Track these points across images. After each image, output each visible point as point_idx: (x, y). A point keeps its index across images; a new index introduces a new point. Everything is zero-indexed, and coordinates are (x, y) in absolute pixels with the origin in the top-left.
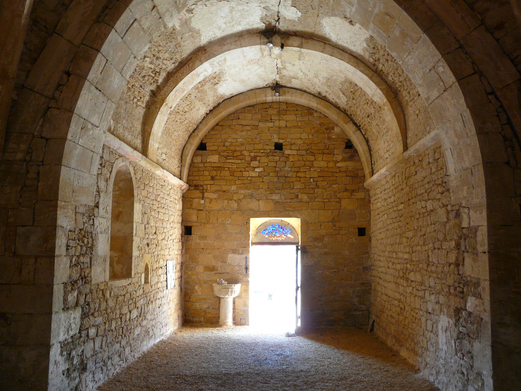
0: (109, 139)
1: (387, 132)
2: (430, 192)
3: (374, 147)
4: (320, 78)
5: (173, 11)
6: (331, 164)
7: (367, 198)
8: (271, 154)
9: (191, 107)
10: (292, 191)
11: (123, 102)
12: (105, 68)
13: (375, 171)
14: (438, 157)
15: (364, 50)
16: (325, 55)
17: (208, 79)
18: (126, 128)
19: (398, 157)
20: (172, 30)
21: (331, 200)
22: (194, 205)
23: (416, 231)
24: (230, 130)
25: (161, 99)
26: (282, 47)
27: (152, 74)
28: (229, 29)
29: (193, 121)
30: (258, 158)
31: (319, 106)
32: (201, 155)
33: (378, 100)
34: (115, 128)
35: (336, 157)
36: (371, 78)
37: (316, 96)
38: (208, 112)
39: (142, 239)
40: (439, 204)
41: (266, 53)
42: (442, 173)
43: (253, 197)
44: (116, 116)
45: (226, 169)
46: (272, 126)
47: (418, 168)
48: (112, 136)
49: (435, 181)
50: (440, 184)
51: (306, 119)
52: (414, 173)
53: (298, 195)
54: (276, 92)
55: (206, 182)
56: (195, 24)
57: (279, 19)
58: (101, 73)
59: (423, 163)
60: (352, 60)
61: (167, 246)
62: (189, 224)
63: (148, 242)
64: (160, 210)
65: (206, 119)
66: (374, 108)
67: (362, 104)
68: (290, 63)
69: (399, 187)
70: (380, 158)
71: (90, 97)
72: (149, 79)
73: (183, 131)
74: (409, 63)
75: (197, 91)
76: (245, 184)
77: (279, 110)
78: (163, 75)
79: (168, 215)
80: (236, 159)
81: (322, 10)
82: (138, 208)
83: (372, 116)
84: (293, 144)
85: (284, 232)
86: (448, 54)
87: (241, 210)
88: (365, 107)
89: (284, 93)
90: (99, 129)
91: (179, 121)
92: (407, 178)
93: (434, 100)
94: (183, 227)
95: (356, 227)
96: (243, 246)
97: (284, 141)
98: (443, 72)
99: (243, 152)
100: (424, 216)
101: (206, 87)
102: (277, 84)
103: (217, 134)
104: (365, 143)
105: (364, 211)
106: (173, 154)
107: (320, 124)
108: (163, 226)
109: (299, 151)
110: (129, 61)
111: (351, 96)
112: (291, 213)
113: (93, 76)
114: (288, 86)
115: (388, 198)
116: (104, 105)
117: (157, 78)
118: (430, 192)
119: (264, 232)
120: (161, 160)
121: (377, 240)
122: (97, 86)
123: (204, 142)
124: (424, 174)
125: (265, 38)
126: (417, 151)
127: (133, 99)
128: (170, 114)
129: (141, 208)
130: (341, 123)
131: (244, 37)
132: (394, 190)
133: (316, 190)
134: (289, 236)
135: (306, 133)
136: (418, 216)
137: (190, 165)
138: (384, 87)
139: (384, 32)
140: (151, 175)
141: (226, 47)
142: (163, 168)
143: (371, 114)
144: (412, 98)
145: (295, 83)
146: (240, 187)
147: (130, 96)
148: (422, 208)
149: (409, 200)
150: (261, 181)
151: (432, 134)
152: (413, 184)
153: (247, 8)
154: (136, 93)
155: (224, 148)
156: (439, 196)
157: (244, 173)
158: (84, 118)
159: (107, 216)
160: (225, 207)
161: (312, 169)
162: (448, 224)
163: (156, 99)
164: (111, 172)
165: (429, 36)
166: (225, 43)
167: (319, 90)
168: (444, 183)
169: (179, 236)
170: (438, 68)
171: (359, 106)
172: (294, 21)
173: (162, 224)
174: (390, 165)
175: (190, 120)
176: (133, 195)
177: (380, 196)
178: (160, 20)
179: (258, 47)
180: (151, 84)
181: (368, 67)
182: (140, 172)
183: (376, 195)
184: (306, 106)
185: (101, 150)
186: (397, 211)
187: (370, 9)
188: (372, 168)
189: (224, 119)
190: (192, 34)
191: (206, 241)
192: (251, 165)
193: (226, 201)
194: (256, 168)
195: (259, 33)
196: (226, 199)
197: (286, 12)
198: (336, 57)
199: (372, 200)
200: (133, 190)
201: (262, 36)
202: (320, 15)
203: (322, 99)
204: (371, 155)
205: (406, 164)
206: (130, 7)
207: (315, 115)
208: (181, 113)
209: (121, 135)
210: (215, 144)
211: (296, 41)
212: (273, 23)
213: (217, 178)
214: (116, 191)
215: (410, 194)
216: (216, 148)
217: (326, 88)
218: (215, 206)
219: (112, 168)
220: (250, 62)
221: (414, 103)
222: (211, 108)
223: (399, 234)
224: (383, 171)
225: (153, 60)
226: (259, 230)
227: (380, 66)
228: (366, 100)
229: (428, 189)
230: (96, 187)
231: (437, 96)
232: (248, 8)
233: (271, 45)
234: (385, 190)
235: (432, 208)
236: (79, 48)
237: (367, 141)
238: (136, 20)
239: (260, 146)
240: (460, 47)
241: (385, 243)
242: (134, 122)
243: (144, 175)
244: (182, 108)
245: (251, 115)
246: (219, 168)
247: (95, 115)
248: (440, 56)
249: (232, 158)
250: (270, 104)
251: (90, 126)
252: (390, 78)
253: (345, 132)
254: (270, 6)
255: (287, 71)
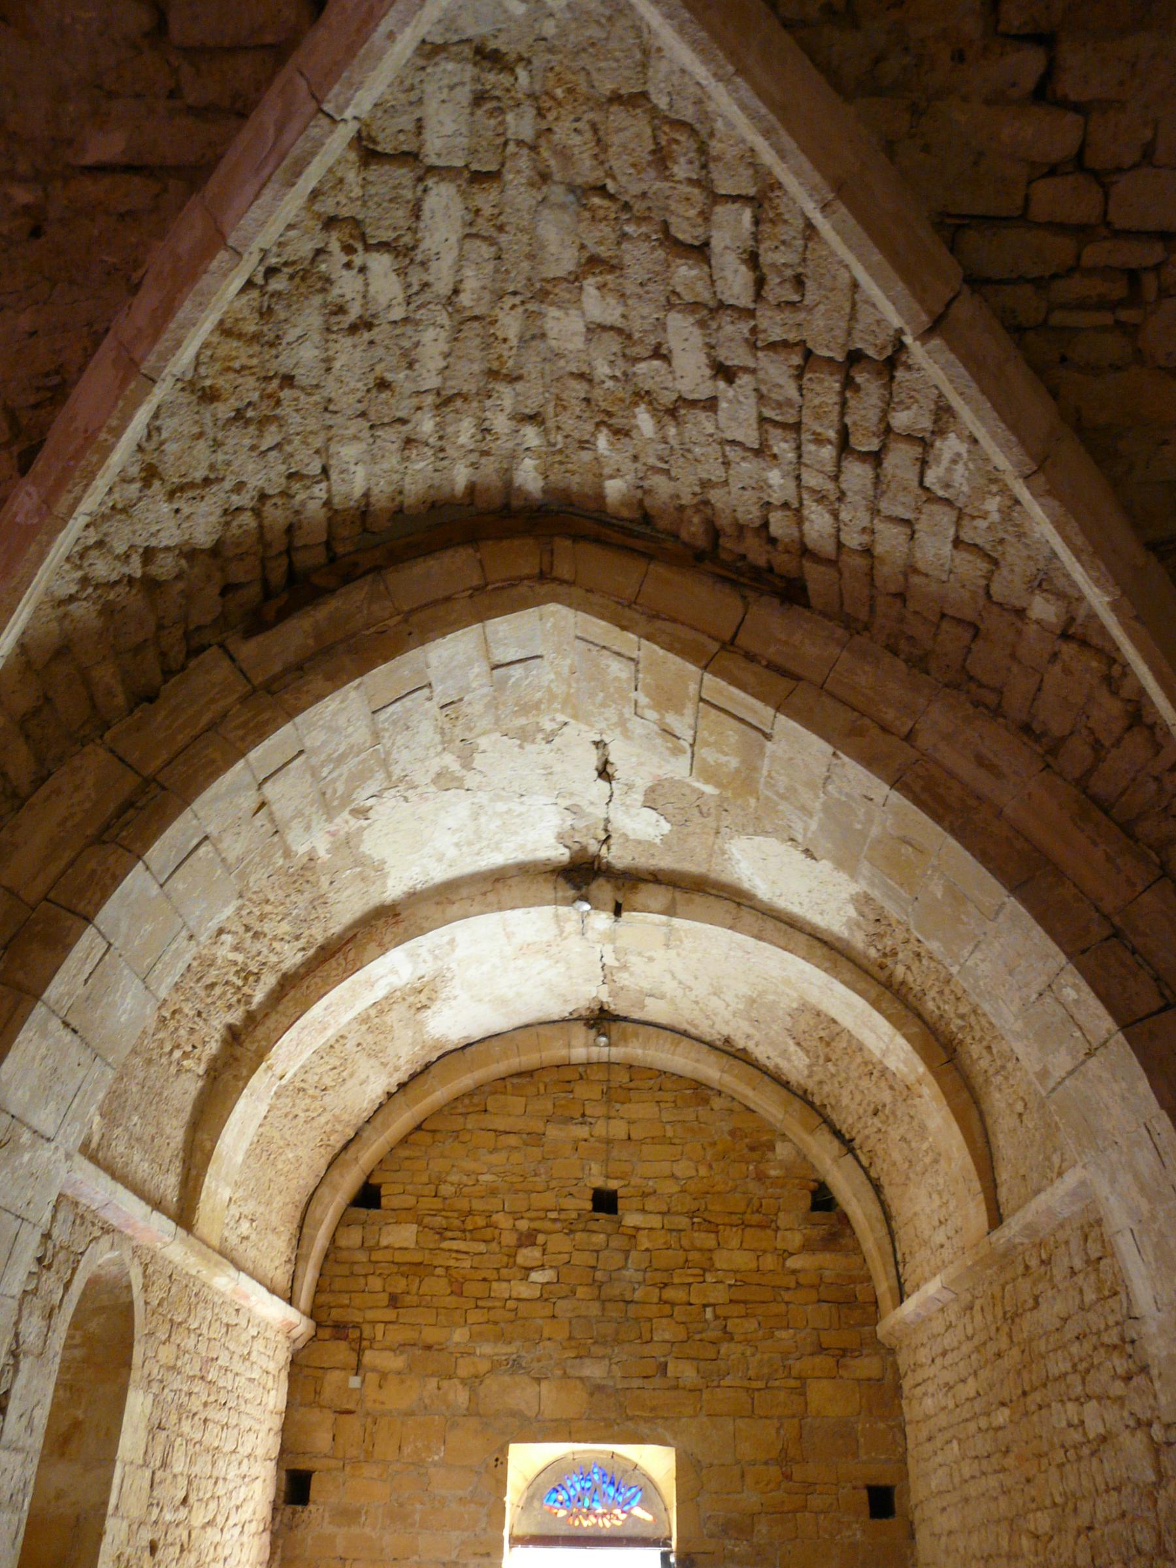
0: (78, 1176)
1: (936, 1161)
2: (1088, 1371)
3: (901, 1208)
4: (729, 997)
5: (314, 817)
6: (769, 1262)
7: (889, 1376)
8: (581, 1226)
9: (344, 1074)
10: (647, 1350)
11: (138, 1061)
12: (100, 968)
13: (907, 1287)
14: (1099, 1254)
15: (851, 924)
16: (739, 937)
17: (398, 994)
18: (138, 1140)
19: (976, 1245)
20: (305, 860)
21: (771, 1383)
22: (328, 1393)
23: (1059, 1510)
24: (456, 1144)
25: (256, 1051)
26: (618, 911)
27: (234, 979)
28: (468, 860)
29: (345, 1117)
30: (541, 1238)
31: (727, 1078)
32: (363, 1224)
33: (901, 1066)
34: (105, 1143)
35: (783, 1240)
36: (875, 1004)
37: (716, 1048)
38: (394, 1090)
39: (135, 1527)
40: (1122, 1418)
41: (571, 927)
42: (1116, 1307)
43: (521, 1367)
44: (110, 1103)
45: (439, 1271)
46: (586, 1136)
47: (1040, 1286)
48: (90, 1168)
49: (1098, 1333)
50: (1115, 1347)
51: (689, 1114)
52: (1031, 1303)
53: (666, 1364)
54: (600, 1034)
55: (371, 1315)
56: (373, 845)
57: (609, 837)
58: (86, 981)
59: (1055, 1272)
60: (819, 952)
61: (219, 1548)
62: (302, 1465)
63: (156, 1537)
64: (212, 1413)
65: (385, 1110)
66: (891, 1088)
67: (854, 1074)
68: (640, 954)
69: (989, 1344)
70: (920, 1246)
71: (43, 1050)
72: (224, 993)
73: (312, 1145)
74: (979, 973)
75: (364, 1027)
76: (496, 1323)
77: (609, 1088)
78: (269, 981)
79: (236, 1431)
80: (473, 1240)
81: (727, 820)
82: (139, 1409)
83: (887, 1111)
84: (649, 1194)
85: (620, 1499)
86: (1083, 952)
87: (478, 1414)
88: (865, 1083)
89: (624, 1039)
90: (53, 1145)
91: (302, 1115)
92: (1012, 1317)
93: (1064, 1079)
94: (284, 1475)
95: (860, 1483)
96: (483, 1550)
97: (622, 1183)
98: (1076, 1001)
99: (495, 1217)
100: (1079, 1459)
101: (391, 1018)
102: (601, 1010)
103: (418, 1158)
104: (870, 1194)
105: (882, 1425)
106: (275, 1220)
107: (732, 1133)
108: (215, 1474)
109: (667, 1218)
110: (174, 947)
111: (822, 1050)
112: (644, 1429)
113: (62, 989)
114: (636, 1015)
115: (956, 1383)
116: (81, 1073)
117: (249, 992)
118: (1088, 1371)
119: (554, 1496)
120: (234, 1240)
121: (933, 1535)
122: (69, 1019)
123: (373, 1181)
124: (1059, 1307)
125: (568, 886)
126: (1030, 1229)
127: (171, 1052)
128: (278, 1095)
129: (148, 1412)
130: (796, 1131)
131: (509, 882)
132: (974, 1357)
133: (724, 1348)
134: (638, 1512)
135: (690, 1159)
136: (1059, 1456)
137: (326, 1256)
138: (916, 1030)
139: (901, 885)
140: (195, 1290)
141: (455, 909)
142: (239, 1268)
143: (884, 1106)
144: (999, 1063)
145: (655, 1010)
146: (481, 1334)
147: (162, 1041)
148: (1070, 1425)
149: (1025, 1394)
150: (548, 1312)
151: (1071, 1179)
152: (1031, 1340)
153: (519, 809)
154: (183, 1032)
155: (437, 1204)
156: (1118, 1388)
157: (495, 1285)
158: (13, 1112)
159: (30, 1441)
160: (427, 1401)
161: (709, 1278)
162: (1162, 1492)
163: (238, 1051)
164: (67, 1286)
165: (1024, 901)
166: (453, 897)
167: (726, 1031)
168: (1126, 1345)
169: (265, 1511)
170: (1060, 990)
171: (847, 1079)
172: (652, 845)
173: (214, 1464)
174: (951, 1271)
175: (337, 1111)
176: (127, 1364)
177: (929, 1372)
178: (276, 838)
179: (549, 910)
180: (230, 1007)
181: (866, 972)
182: (162, 1281)
183: (919, 1371)
184: (689, 1075)
185: (47, 1215)
186: (991, 1433)
187: (859, 827)
188: (899, 1277)
189: (439, 1112)
190: (361, 873)
191: (355, 1530)
192: (520, 1260)
193: (432, 1383)
194: (532, 1269)
195: (553, 871)
196: (432, 1375)
197: (627, 821)
198: (771, 942)
199: (907, 1384)
200: (131, 1346)
201: (561, 881)
202: (724, 830)
203: (736, 1057)
204: (891, 1234)
205: (1002, 1268)
206: (196, 805)
207: (717, 1103)
208: (311, 1092)
209: (119, 1162)
210: (409, 1188)
211: (659, 896)
212: (593, 847)
213: (408, 1299)
214: (76, 1346)
215: (1025, 1375)
216: (410, 1201)
217: (745, 1027)
218: (396, 1398)
219: (74, 1270)
220: (525, 949)
221: (1006, 1078)
222: (402, 1076)
223: (1006, 1518)
224: (932, 1288)
225: (242, 941)
226: (538, 1490)
227: (900, 971)
228: (866, 1064)
229: (1081, 1360)
230: (9, 1338)
231: (1069, 1067)
232: (523, 809)
233: (586, 907)
234: (944, 1354)
235: (1101, 1430)
236: (33, 909)
237: (877, 1188)
238: (206, 838)
239: (548, 1199)
240: (1114, 936)
241: (961, 1550)
242: (165, 1120)
243: (173, 1290)
244: (316, 1078)
245: (523, 1100)
246: (418, 1269)
247: (47, 1103)
248: (1062, 959)
249: (458, 1234)
250: (581, 1069)
251: (26, 1137)
252: (931, 1005)
253: (810, 1158)
254: (584, 804)
255: (632, 974)
